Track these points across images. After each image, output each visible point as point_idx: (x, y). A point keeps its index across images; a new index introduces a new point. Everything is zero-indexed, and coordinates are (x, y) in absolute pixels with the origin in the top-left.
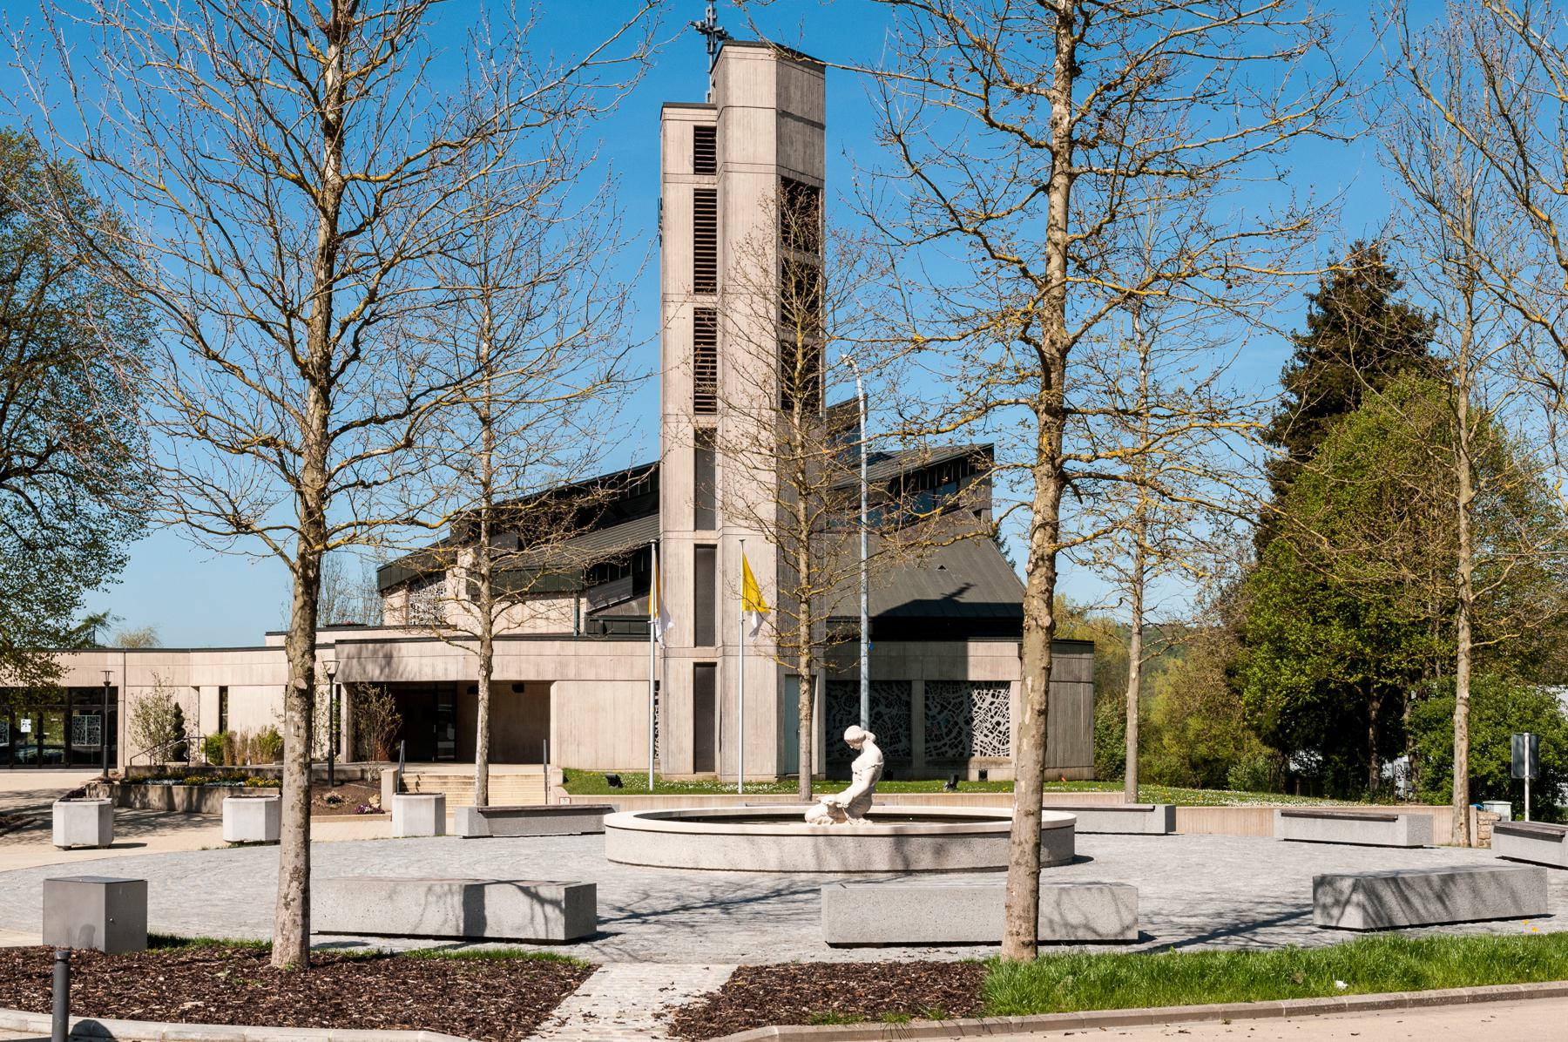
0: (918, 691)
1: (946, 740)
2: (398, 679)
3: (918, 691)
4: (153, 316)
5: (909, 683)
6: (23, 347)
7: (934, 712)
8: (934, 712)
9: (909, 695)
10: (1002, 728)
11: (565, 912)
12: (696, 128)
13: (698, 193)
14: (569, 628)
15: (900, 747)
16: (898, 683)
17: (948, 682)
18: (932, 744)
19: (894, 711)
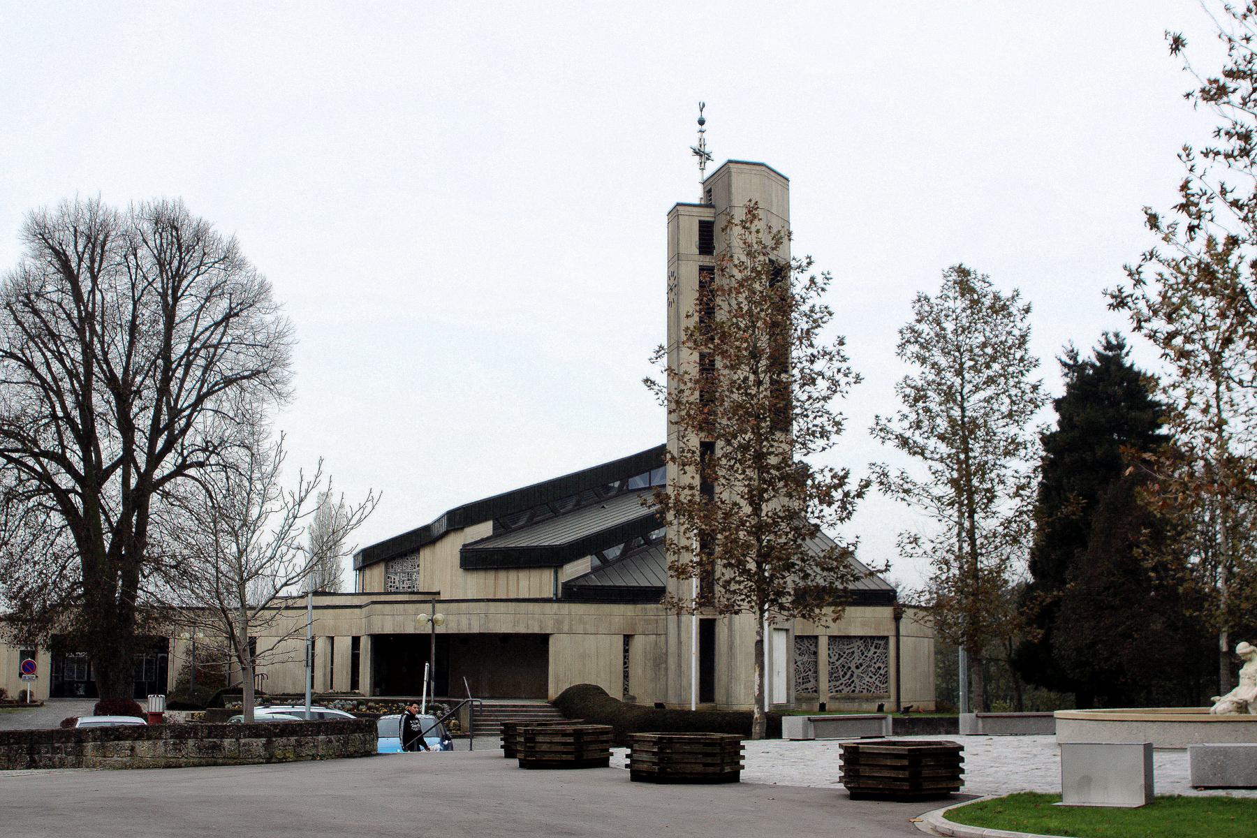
0: (823, 642)
1: (842, 680)
2: (735, 708)
3: (823, 642)
4: (199, 440)
5: (816, 637)
6: (1220, 411)
7: (834, 659)
8: (834, 659)
9: (816, 646)
10: (882, 672)
11: (62, 512)
12: (700, 222)
13: (702, 269)
14: (549, 593)
15: (809, 685)
16: (808, 637)
17: (844, 637)
18: (833, 683)
19: (805, 658)
